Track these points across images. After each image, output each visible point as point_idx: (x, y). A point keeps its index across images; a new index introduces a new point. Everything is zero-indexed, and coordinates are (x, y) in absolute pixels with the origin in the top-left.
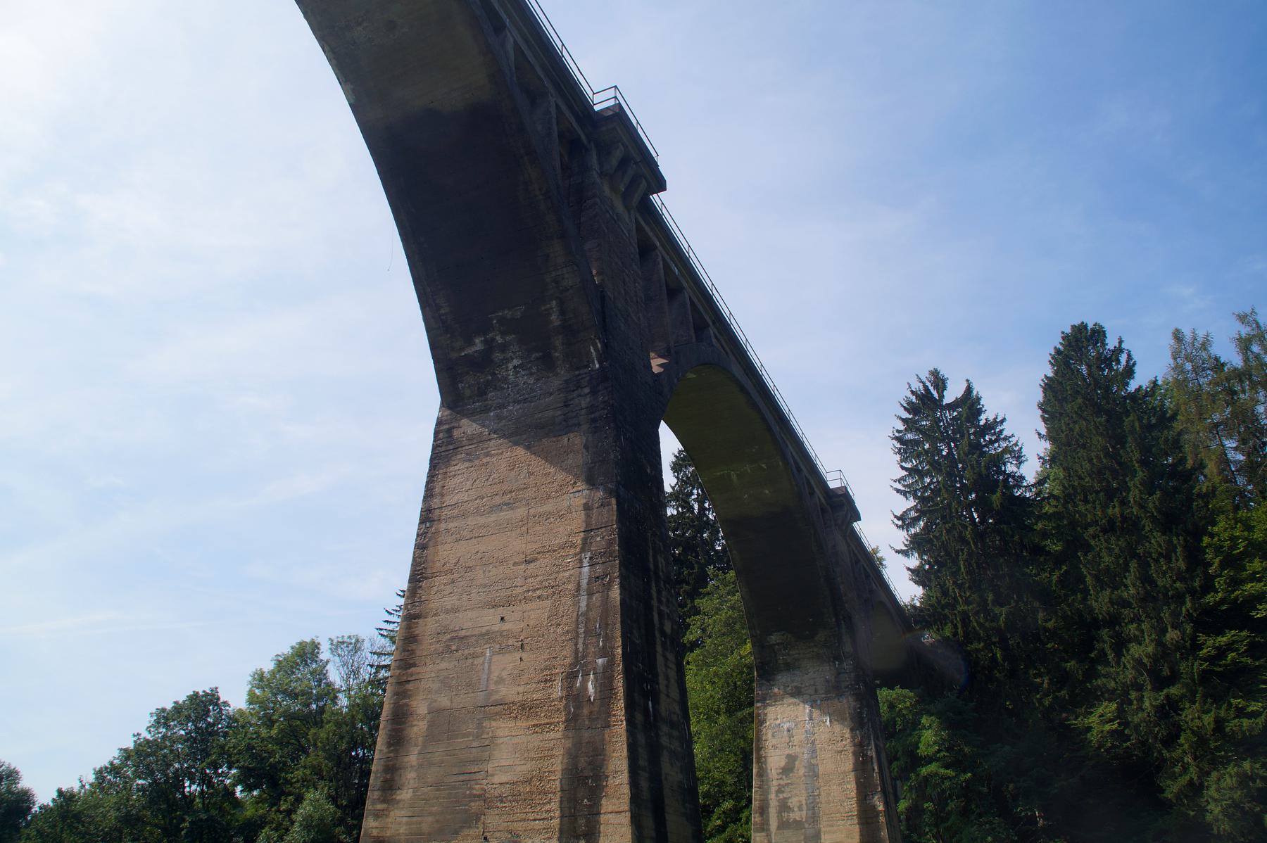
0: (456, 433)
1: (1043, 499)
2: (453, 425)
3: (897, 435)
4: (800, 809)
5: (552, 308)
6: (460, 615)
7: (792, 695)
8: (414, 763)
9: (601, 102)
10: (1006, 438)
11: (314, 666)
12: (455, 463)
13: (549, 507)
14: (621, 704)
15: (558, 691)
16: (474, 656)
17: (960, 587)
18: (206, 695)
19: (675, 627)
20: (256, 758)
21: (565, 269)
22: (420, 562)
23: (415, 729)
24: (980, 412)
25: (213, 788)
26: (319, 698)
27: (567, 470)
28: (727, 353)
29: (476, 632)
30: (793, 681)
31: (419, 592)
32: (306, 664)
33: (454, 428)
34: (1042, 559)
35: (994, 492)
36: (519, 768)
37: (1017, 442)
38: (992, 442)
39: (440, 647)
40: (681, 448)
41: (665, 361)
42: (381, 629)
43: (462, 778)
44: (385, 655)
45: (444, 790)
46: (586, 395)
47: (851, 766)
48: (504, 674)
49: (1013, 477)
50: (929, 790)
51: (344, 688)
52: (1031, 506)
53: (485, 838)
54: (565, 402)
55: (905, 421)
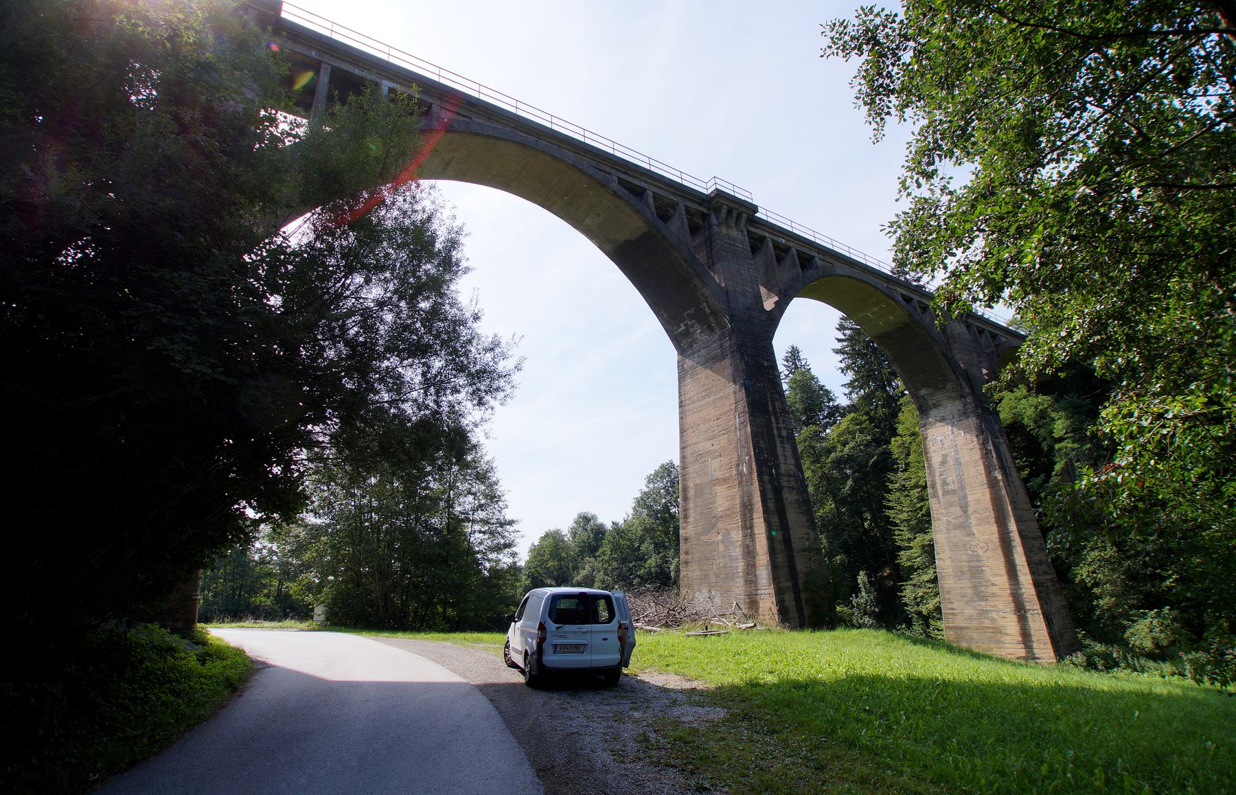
0: (685, 366)
7: (940, 422)
9: (706, 188)
13: (721, 394)
15: (734, 472)
16: (705, 461)
18: (668, 464)
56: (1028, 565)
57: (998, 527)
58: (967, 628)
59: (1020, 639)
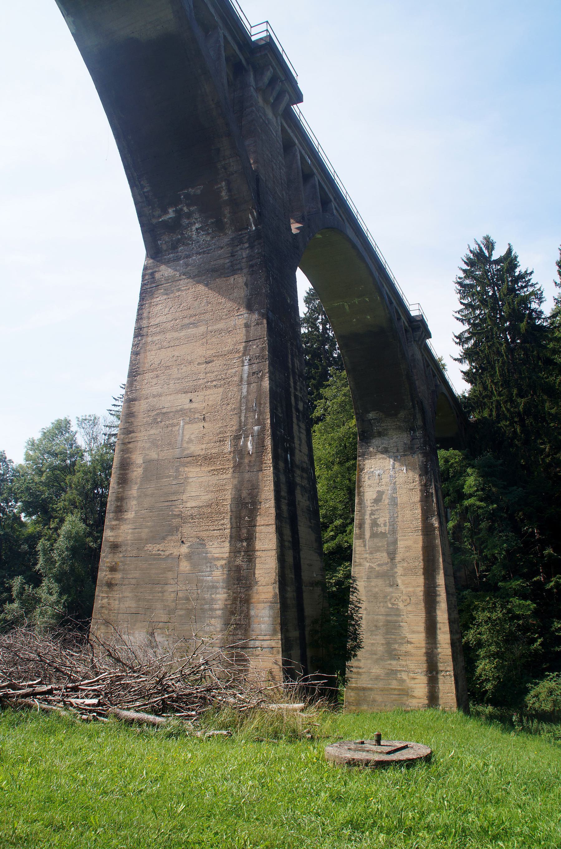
0: (157, 276)
1: (555, 327)
2: (155, 270)
3: (459, 280)
4: (385, 525)
5: (222, 187)
6: (163, 398)
7: (382, 453)
8: (135, 495)
10: (532, 285)
11: (67, 435)
12: (156, 296)
14: (270, 456)
15: (228, 447)
16: (173, 425)
17: (496, 384)
19: (306, 406)
20: (33, 496)
21: (231, 159)
22: (135, 364)
23: (135, 473)
24: (516, 266)
25: (6, 514)
26: (72, 456)
27: (233, 300)
28: (343, 220)
29: (174, 410)
30: (382, 444)
31: (135, 383)
32: (62, 434)
33: (155, 272)
34: (551, 368)
35: (522, 321)
36: (203, 498)
37: (540, 288)
38: (522, 287)
39: (150, 420)
40: (311, 287)
41: (300, 225)
42: (110, 410)
43: (166, 504)
44: (114, 427)
45: (155, 511)
46: (246, 249)
47: (419, 499)
48: (192, 436)
49: (536, 311)
50: (469, 515)
51: (88, 449)
52: (546, 331)
53: (183, 542)
54: (231, 254)
55: (465, 271)
56: (449, 623)
57: (425, 579)
58: (371, 689)
59: (427, 702)
